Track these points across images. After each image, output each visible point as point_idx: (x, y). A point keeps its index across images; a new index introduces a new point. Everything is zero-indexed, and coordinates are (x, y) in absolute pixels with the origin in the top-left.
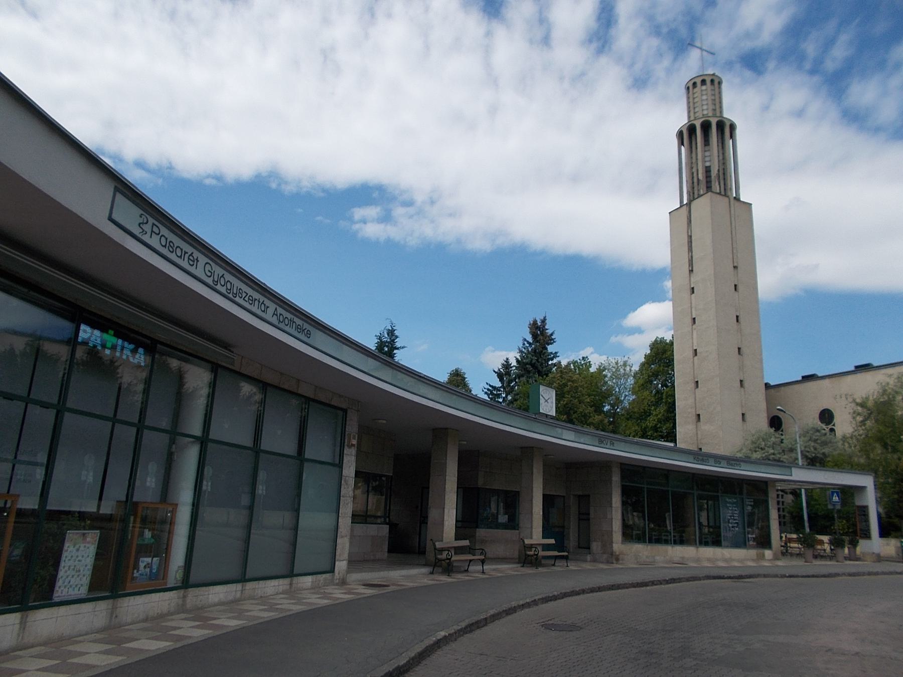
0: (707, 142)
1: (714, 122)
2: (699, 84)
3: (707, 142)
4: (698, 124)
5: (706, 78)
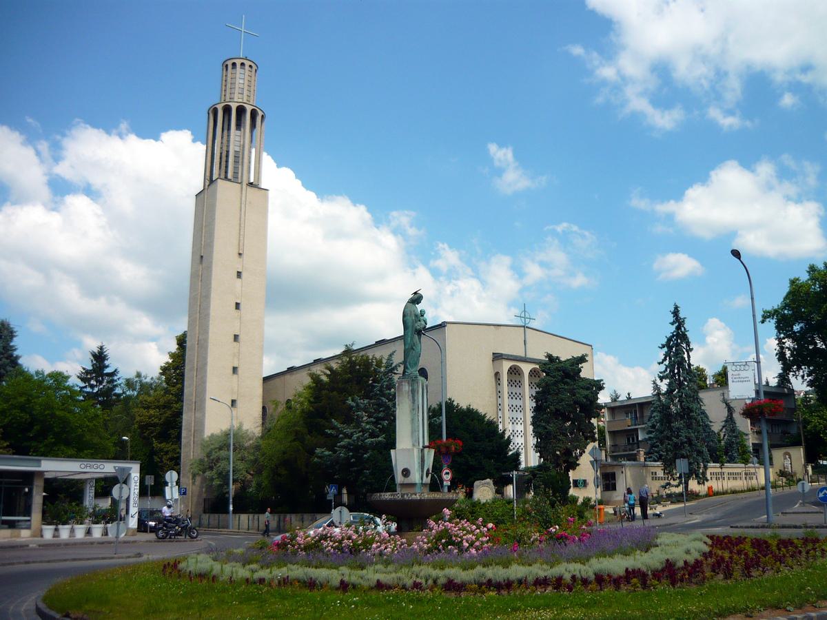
0: (239, 125)
1: (249, 108)
2: (238, 66)
3: (239, 125)
4: (234, 106)
5: (245, 61)
